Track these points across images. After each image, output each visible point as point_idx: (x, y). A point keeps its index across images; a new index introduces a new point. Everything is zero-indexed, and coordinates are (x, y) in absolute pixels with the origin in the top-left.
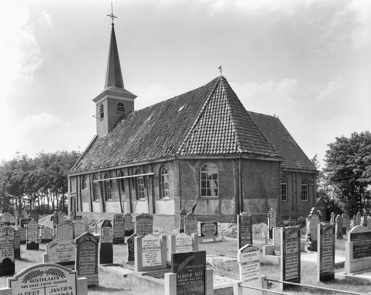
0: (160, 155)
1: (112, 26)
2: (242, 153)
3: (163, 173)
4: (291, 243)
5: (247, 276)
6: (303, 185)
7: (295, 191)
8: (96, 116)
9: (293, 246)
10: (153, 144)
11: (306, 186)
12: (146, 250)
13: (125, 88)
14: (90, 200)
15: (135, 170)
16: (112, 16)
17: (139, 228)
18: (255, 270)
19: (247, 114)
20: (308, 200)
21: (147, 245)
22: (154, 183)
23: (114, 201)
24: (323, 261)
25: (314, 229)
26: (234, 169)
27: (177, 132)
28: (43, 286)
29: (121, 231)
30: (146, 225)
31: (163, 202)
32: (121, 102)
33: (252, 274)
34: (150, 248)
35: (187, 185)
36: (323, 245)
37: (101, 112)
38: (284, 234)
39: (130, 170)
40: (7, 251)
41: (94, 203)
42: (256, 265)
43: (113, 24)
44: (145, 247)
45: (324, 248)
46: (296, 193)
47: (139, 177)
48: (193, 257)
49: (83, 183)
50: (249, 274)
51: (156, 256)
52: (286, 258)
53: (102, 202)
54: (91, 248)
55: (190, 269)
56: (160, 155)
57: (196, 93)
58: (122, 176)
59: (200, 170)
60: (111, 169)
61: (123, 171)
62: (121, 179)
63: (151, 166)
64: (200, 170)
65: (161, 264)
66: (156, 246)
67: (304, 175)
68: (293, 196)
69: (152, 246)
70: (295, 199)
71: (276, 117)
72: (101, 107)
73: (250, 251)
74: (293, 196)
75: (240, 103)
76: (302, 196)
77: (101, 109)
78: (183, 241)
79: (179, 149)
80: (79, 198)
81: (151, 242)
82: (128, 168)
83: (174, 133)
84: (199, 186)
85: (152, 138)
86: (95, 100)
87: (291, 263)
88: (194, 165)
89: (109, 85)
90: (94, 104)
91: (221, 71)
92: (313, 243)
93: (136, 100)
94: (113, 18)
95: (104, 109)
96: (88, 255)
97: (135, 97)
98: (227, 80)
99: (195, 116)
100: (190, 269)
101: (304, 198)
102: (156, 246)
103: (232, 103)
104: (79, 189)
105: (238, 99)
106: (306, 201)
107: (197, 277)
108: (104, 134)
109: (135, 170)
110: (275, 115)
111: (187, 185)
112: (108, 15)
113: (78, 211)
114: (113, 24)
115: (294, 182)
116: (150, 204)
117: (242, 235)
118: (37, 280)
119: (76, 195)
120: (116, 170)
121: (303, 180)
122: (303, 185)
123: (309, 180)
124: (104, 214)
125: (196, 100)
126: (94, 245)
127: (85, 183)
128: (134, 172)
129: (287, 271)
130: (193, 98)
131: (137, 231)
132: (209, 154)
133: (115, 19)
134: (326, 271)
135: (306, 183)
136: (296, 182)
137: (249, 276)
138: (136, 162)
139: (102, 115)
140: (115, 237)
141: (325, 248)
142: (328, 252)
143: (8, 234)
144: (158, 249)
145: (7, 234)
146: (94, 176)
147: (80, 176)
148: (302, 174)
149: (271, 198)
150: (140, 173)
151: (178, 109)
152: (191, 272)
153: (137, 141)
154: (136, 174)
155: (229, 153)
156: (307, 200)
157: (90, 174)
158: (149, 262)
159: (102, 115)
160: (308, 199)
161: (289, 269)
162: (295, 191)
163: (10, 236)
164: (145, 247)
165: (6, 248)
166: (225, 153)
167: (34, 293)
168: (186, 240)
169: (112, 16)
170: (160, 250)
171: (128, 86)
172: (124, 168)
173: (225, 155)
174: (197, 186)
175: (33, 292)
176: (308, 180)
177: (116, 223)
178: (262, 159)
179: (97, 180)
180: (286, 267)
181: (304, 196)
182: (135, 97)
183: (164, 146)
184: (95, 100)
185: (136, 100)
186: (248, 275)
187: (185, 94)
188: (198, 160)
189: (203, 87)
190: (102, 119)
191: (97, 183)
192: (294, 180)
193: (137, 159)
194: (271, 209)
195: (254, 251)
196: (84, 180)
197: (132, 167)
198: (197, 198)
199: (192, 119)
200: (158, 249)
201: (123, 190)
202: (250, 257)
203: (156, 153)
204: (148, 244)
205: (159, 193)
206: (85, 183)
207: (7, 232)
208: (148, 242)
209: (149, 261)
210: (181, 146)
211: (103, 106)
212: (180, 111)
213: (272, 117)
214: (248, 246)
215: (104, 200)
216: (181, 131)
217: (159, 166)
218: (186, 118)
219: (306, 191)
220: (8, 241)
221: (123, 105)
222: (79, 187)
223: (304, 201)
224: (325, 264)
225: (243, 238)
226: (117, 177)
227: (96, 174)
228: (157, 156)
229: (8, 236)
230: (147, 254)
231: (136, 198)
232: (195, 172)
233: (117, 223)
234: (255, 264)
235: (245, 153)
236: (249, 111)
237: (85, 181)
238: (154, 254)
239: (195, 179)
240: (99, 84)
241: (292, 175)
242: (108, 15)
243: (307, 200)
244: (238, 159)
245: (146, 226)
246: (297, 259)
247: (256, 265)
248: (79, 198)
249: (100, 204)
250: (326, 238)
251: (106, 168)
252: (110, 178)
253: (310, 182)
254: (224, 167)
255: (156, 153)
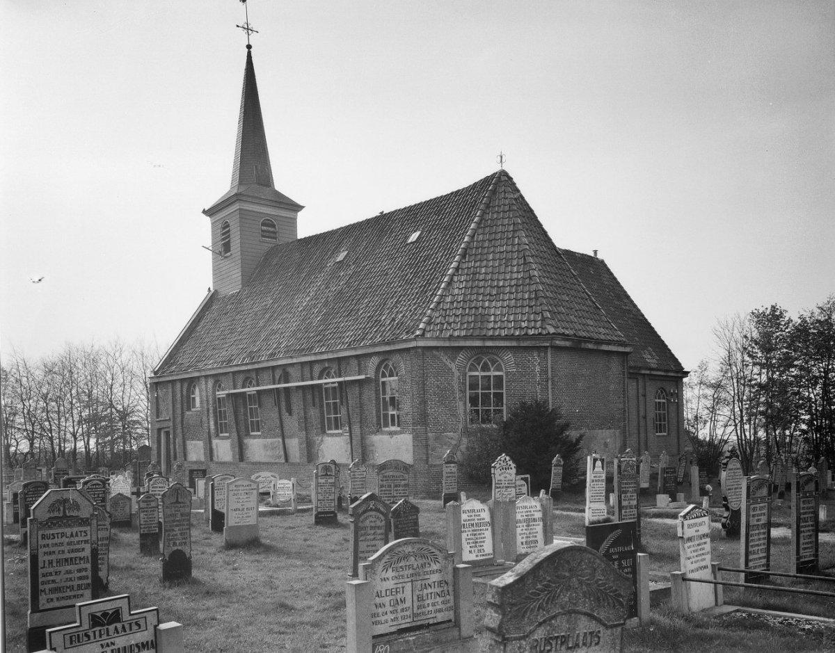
0: (378, 337)
1: (247, 50)
2: (554, 334)
3: (384, 375)
4: (758, 505)
5: (692, 563)
6: (657, 400)
7: (642, 413)
8: (211, 248)
9: (760, 512)
10: (356, 313)
11: (664, 403)
12: (467, 529)
13: (277, 188)
14: (206, 435)
15: (317, 369)
16: (248, 29)
17: (384, 489)
18: (703, 552)
19: (557, 252)
20: (669, 434)
21: (468, 518)
22: (365, 397)
23: (265, 437)
24: (802, 541)
25: (734, 487)
26: (538, 369)
27: (412, 289)
28: (410, 580)
29: (330, 498)
30: (397, 482)
31: (386, 437)
32: (269, 220)
33: (700, 558)
34: (473, 525)
35: (439, 401)
36: (802, 511)
37: (223, 239)
38: (748, 488)
39: (307, 369)
40: (176, 535)
41: (215, 442)
42: (705, 543)
43: (249, 47)
44: (465, 523)
45: (802, 516)
46: (645, 417)
47: (326, 384)
48: (619, 531)
49: (188, 397)
50: (696, 559)
51: (482, 540)
52: (751, 533)
53: (236, 440)
54: (378, 523)
55: (615, 554)
56: (378, 337)
57: (445, 205)
58: (287, 381)
59: (467, 370)
60: (261, 366)
61: (290, 370)
62: (285, 388)
63: (356, 362)
64: (467, 370)
65: (492, 556)
66: (483, 521)
67: (661, 380)
68: (639, 423)
69: (477, 521)
70: (642, 430)
71: (600, 256)
72: (224, 228)
73: (697, 517)
74: (639, 423)
75: (543, 229)
76: (657, 424)
77: (223, 234)
78: (527, 512)
79: (421, 326)
80: (179, 431)
81: (474, 513)
82: (302, 364)
83: (405, 289)
84: (465, 404)
85: (353, 300)
86: (209, 213)
87: (757, 543)
88: (453, 359)
89: (241, 183)
90: (207, 221)
91: (501, 157)
92: (732, 513)
93: (301, 216)
94: (250, 32)
95: (231, 233)
96: (372, 537)
97: (297, 208)
98: (515, 180)
99: (450, 256)
100: (615, 554)
101: (660, 428)
102: (483, 521)
103: (527, 230)
104: (179, 411)
105: (539, 222)
106: (664, 436)
107: (625, 567)
108: (233, 287)
109: (317, 369)
110: (595, 252)
111: (439, 401)
112: (238, 26)
113: (175, 458)
114: (249, 47)
115: (640, 395)
116: (354, 442)
117: (623, 498)
118: (401, 567)
119: (171, 424)
120: (273, 368)
121: (657, 392)
122: (657, 400)
123: (670, 391)
124: (242, 465)
125: (446, 220)
126: (383, 518)
127: (193, 396)
128: (316, 374)
129: (751, 557)
130: (439, 216)
131: (593, 478)
132: (512, 335)
133: (253, 35)
134: (806, 559)
135: (664, 398)
136: (644, 396)
137: (696, 562)
138: (321, 354)
139: (227, 247)
140: (319, 510)
141: (804, 516)
142: (807, 524)
143: (179, 500)
144: (487, 528)
145: (177, 502)
146: (216, 382)
147: (182, 381)
148: (657, 378)
149: (610, 428)
150: (328, 376)
151: (407, 238)
152: (615, 560)
153: (315, 306)
154: (320, 378)
155: (526, 334)
156: (665, 434)
157: (206, 377)
158: (473, 551)
159: (227, 247)
160: (668, 431)
161: (754, 553)
162: (642, 413)
163: (182, 505)
164: (465, 523)
165: (177, 529)
166: (518, 336)
167: (398, 590)
168: (531, 509)
169: (248, 29)
170: (490, 528)
171: (284, 181)
172: (292, 365)
173: (518, 338)
174: (461, 404)
175: (396, 589)
176: (668, 391)
177: (320, 481)
178: (590, 346)
179: (223, 390)
180: (750, 549)
181: (660, 424)
182: (297, 208)
183: (384, 318)
184: (209, 213)
185: (300, 215)
186: (694, 560)
187: (419, 204)
188: (461, 348)
189: (459, 191)
190: (229, 254)
191: (223, 398)
192: (641, 391)
193: (323, 345)
194: (627, 451)
195: (701, 516)
196: (190, 391)
197: (311, 363)
198: (460, 428)
199: (443, 262)
200: (487, 528)
201: (290, 412)
202: (696, 528)
203: (367, 333)
204: (469, 518)
205: (375, 419)
206: (193, 396)
207: (177, 497)
208: (470, 514)
209: (473, 549)
210: (425, 319)
211: (228, 226)
212: (411, 243)
213: (591, 257)
214: (692, 509)
215: (243, 433)
216: (420, 287)
217: (375, 361)
218: (427, 258)
219: (329, 413)
220: (179, 516)
221: (274, 226)
222: (179, 406)
223: (661, 434)
224: (805, 546)
225: (624, 503)
226: (274, 384)
227: (223, 378)
228: (371, 339)
229: (179, 505)
230: (469, 537)
231: (319, 430)
232: (457, 374)
233: (323, 481)
234: (703, 540)
235: (559, 334)
236: (561, 248)
237: (193, 393)
238: (481, 536)
239: (456, 387)
240: (218, 175)
241: (638, 381)
242: (238, 26)
243: (665, 434)
244: (546, 347)
245: (396, 486)
246: (766, 536)
247: (705, 543)
248: (179, 431)
249: (232, 445)
250: (804, 499)
251: (247, 364)
252: (258, 385)
253: (672, 394)
254: (517, 365)
255: (367, 333)
